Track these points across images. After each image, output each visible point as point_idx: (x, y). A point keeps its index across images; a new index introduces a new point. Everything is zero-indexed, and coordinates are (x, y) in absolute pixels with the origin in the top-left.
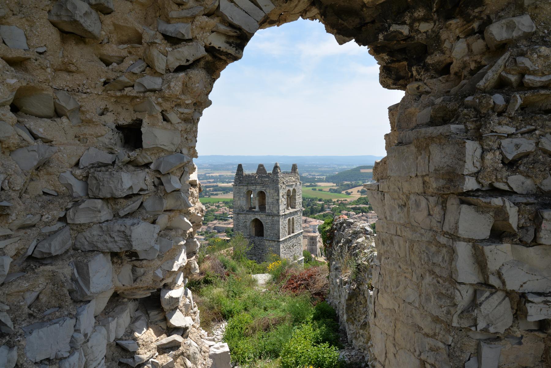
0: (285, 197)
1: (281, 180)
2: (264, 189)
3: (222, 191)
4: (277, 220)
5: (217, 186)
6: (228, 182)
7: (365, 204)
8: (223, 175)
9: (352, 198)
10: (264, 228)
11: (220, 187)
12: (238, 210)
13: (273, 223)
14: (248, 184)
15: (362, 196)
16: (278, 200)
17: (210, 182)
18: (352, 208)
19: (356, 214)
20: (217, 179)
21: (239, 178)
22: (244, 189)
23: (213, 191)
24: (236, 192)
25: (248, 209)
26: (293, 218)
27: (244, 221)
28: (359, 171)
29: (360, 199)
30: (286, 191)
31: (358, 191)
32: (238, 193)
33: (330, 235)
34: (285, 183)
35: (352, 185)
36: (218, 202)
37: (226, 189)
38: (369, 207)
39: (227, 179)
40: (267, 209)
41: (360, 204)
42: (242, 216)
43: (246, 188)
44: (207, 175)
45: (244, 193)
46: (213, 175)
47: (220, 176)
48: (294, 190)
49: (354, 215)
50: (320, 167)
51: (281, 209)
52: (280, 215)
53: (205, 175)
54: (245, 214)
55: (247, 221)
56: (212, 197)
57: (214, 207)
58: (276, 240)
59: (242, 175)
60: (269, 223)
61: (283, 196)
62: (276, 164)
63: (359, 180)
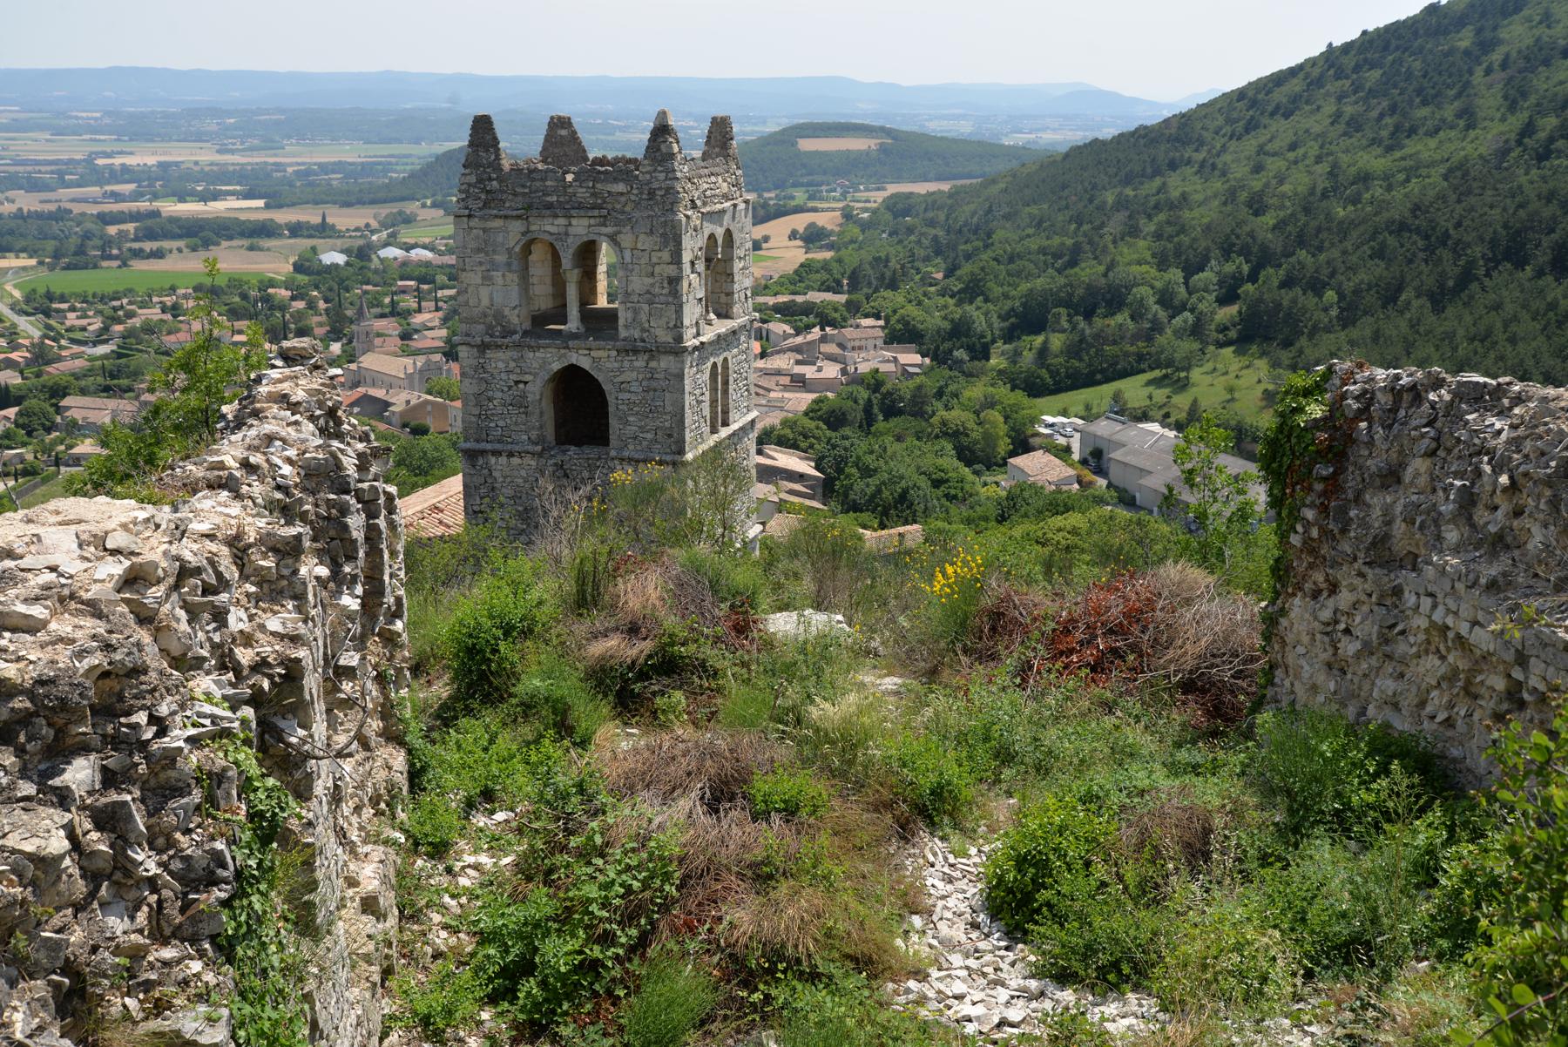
0: (701, 267)
1: (688, 191)
2: (609, 230)
3: (180, 237)
4: (674, 370)
5: (156, 214)
6: (205, 198)
7: (828, 290)
8: (177, 164)
9: (768, 264)
10: (611, 409)
11: (174, 220)
12: (481, 327)
13: (654, 384)
14: (529, 207)
15: (810, 256)
16: (675, 281)
17: (117, 197)
18: (778, 309)
19: (798, 334)
20: (175, 182)
21: (480, 181)
22: (513, 233)
23: (136, 239)
24: (473, 245)
25: (527, 325)
26: (726, 360)
27: (514, 377)
28: (794, 144)
29: (806, 267)
30: (701, 241)
31: (793, 235)
32: (479, 250)
33: (1331, 438)
34: (699, 203)
35: (765, 205)
36: (173, 289)
37: (202, 228)
38: (848, 304)
39: (198, 181)
40: (621, 322)
41: (809, 288)
42: (500, 354)
43: (516, 227)
44: (100, 162)
45: (509, 251)
46: (131, 161)
47: (161, 165)
48: (728, 233)
49: (786, 336)
50: (624, 129)
51: (686, 322)
52: (685, 349)
53: (89, 160)
54: (518, 346)
55: (527, 378)
56: (139, 265)
57: (154, 314)
58: (668, 458)
59: (499, 168)
60: (635, 387)
61: (693, 263)
62: (663, 115)
63: (795, 185)
